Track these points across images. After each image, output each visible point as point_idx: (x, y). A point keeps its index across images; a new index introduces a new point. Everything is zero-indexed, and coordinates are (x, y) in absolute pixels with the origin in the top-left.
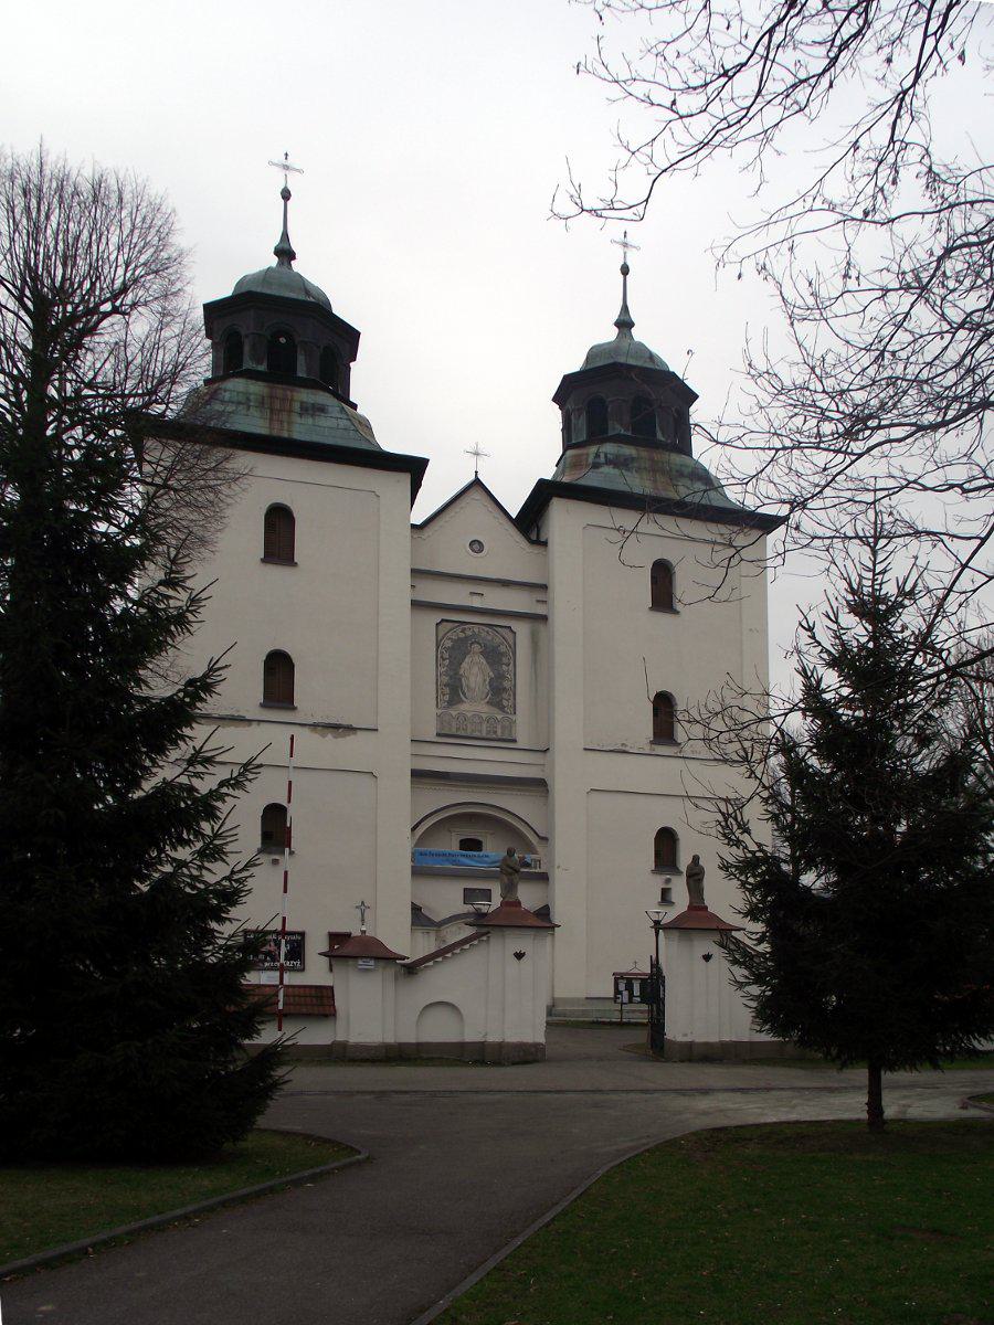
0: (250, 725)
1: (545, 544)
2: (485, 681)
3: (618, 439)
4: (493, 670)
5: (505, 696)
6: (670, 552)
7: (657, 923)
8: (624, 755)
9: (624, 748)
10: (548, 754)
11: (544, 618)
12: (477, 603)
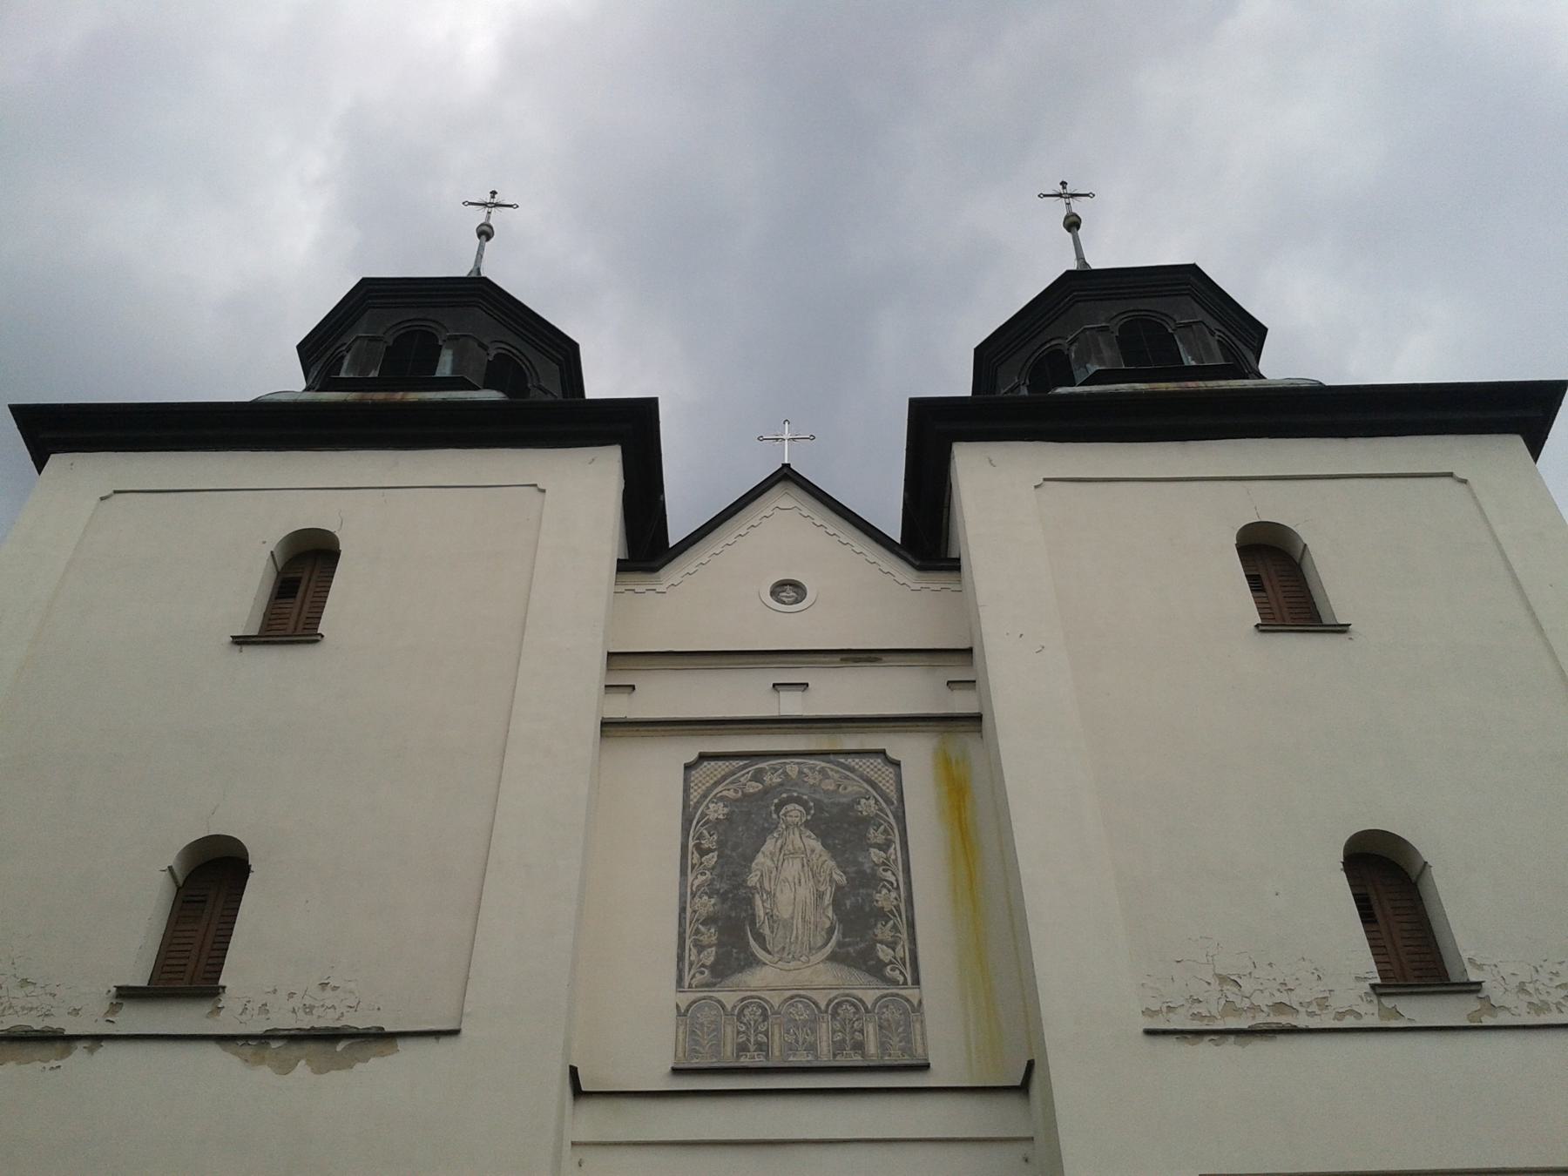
2: (820, 896)
5: (883, 931)
6: (1273, 506)
8: (1281, 1038)
9: (1285, 1020)
12: (791, 705)
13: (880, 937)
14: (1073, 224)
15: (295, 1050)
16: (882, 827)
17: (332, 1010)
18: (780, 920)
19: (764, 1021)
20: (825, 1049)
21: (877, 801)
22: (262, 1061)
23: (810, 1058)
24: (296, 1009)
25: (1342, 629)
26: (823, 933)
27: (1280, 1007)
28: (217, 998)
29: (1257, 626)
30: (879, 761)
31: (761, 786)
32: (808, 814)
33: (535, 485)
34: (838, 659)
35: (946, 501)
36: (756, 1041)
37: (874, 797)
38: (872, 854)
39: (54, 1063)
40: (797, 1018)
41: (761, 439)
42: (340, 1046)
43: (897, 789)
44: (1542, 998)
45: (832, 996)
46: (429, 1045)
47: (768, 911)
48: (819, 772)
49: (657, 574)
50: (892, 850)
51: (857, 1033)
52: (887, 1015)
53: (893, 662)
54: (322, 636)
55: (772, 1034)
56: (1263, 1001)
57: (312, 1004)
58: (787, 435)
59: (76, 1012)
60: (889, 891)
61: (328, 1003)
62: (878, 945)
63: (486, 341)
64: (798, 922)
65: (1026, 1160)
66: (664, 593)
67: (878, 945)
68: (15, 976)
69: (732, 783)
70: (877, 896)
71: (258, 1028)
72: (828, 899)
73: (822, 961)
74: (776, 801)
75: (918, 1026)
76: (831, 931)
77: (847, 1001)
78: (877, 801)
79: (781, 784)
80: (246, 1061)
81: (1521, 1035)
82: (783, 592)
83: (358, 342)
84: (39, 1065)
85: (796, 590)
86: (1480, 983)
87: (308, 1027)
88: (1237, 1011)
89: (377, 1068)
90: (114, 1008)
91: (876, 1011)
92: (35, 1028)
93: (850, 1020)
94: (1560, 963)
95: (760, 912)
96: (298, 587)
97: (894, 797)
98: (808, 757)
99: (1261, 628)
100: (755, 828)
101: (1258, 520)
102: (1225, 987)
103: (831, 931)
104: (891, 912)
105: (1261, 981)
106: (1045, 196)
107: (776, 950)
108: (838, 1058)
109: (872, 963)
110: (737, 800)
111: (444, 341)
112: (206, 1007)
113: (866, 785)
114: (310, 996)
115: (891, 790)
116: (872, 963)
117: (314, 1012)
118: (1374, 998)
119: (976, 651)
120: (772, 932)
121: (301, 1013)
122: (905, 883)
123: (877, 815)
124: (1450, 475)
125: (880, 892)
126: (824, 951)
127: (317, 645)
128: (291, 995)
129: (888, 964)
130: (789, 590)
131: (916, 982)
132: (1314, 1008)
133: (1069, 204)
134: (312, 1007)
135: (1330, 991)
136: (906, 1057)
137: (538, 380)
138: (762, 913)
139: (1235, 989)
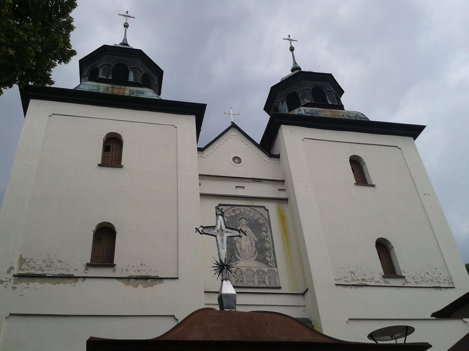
0: (76, 281)
1: (278, 157)
2: (252, 244)
3: (307, 105)
4: (257, 236)
5: (267, 254)
6: (359, 151)
7: (21, 255)
8: (364, 287)
9: (364, 283)
10: (308, 294)
11: (286, 200)
12: (241, 192)
13: (267, 255)
14: (292, 49)
15: (138, 282)
16: (265, 227)
17: (144, 271)
18: (243, 249)
19: (241, 275)
20: (256, 283)
21: (263, 220)
22: (129, 284)
23: (253, 284)
24: (136, 271)
25: (373, 186)
26: (253, 253)
27: (363, 280)
28: (114, 267)
29: (355, 183)
30: (263, 209)
31: (235, 214)
32: (247, 222)
33: (174, 125)
34: (252, 181)
35: (275, 138)
36: (240, 280)
37: (263, 219)
38: (263, 234)
39: (74, 284)
40: (249, 274)
41: (225, 113)
42: (149, 281)
43: (268, 215)
44: (417, 280)
45: (257, 269)
46: (171, 281)
47: (240, 247)
48: (249, 211)
49: (203, 152)
50: (268, 233)
51: (263, 279)
52: (270, 274)
53: (265, 182)
54: (123, 166)
55: (244, 278)
56: (360, 278)
57: (139, 269)
58: (232, 113)
59: (76, 270)
60: (268, 243)
61: (144, 269)
62: (267, 257)
63: (141, 70)
64: (247, 250)
65: (304, 311)
66: (205, 157)
67: (267, 257)
68: (56, 259)
69: (228, 212)
70: (265, 245)
71: (126, 276)
72: (254, 245)
73: (253, 261)
74: (239, 218)
75: (277, 278)
76: (255, 253)
77: (260, 271)
78: (263, 220)
79: (240, 214)
80: (126, 284)
81: (413, 289)
82: (235, 160)
83: (104, 65)
84: (69, 284)
85: (238, 159)
86: (405, 276)
87: (139, 275)
88: (355, 280)
89: (159, 287)
90: (86, 269)
91: (268, 273)
92: (66, 274)
93: (262, 276)
94: (421, 272)
95: (238, 247)
96: (110, 149)
97: (267, 219)
98: (246, 207)
99: (356, 184)
100: (234, 225)
101: (354, 155)
102: (352, 274)
103: (255, 253)
104: (269, 248)
105: (359, 273)
106: (285, 39)
107: (243, 257)
108: (260, 285)
109: (265, 261)
110: (229, 217)
111: (130, 68)
112: (111, 270)
113: (260, 215)
114: (138, 267)
115: (266, 217)
116: (265, 261)
117: (140, 271)
118: (383, 278)
119: (287, 181)
120: (241, 252)
121: (137, 272)
122: (272, 241)
123: (264, 223)
124: (397, 147)
125: (266, 243)
126: (254, 258)
127: (122, 168)
128: (134, 267)
129: (269, 262)
130: (237, 160)
131: (276, 267)
132: (370, 280)
133: (291, 43)
134: (139, 270)
135: (374, 276)
136: (275, 285)
137: (154, 82)
138: (238, 247)
139: (354, 275)
